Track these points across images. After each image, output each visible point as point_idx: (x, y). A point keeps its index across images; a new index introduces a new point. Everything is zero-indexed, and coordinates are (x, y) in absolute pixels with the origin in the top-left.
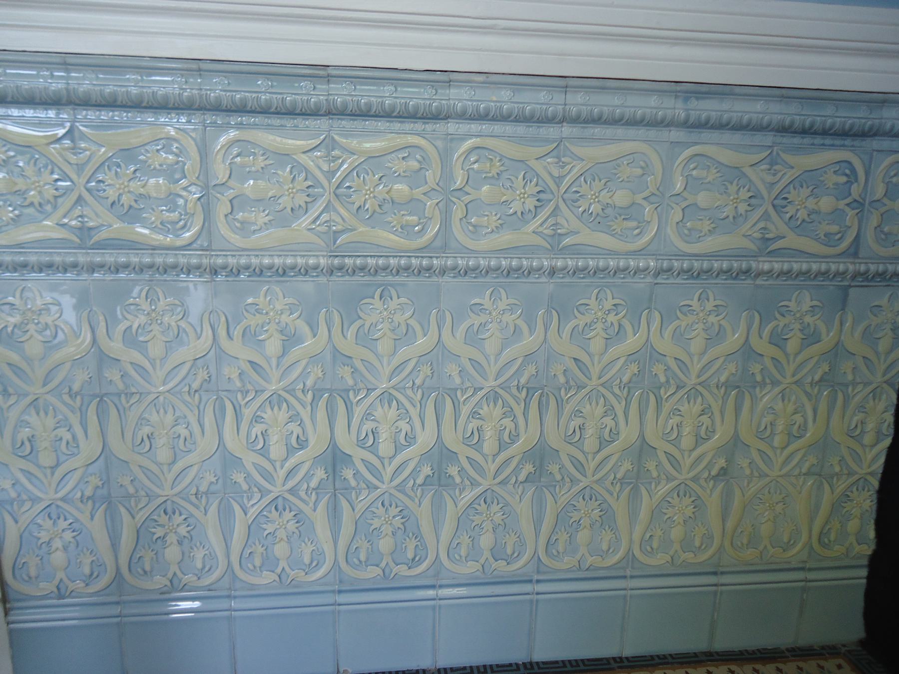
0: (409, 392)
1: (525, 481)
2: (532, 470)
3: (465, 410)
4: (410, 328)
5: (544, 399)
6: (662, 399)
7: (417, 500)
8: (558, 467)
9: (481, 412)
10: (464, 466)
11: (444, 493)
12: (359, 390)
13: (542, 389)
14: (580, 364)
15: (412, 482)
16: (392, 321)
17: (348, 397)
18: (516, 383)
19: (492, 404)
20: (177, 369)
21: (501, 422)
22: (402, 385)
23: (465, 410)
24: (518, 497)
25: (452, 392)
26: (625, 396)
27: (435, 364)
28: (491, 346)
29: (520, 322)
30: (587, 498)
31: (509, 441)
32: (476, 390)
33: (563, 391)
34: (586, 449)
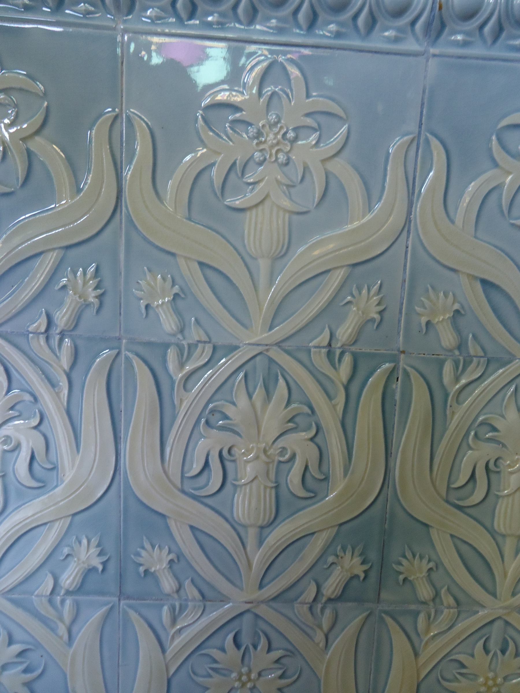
1: (339, 598)
2: (359, 571)
3: (188, 404)
4: (36, 167)
5: (397, 387)
7: (62, 630)
8: (425, 566)
9: (230, 410)
10: (186, 552)
11: (133, 615)
12: (192, 347)
13: (394, 359)
14: (498, 298)
15: (313, 589)
17: (164, 361)
18: (324, 338)
19: (259, 393)
21: (281, 443)
23: (188, 404)
24: (319, 637)
25: (153, 353)
26: (344, 378)
27: (106, 272)
28: (261, 230)
29: (340, 167)
30: (493, 646)
31: (302, 493)
32: (217, 351)
33: (448, 368)
34: (500, 524)
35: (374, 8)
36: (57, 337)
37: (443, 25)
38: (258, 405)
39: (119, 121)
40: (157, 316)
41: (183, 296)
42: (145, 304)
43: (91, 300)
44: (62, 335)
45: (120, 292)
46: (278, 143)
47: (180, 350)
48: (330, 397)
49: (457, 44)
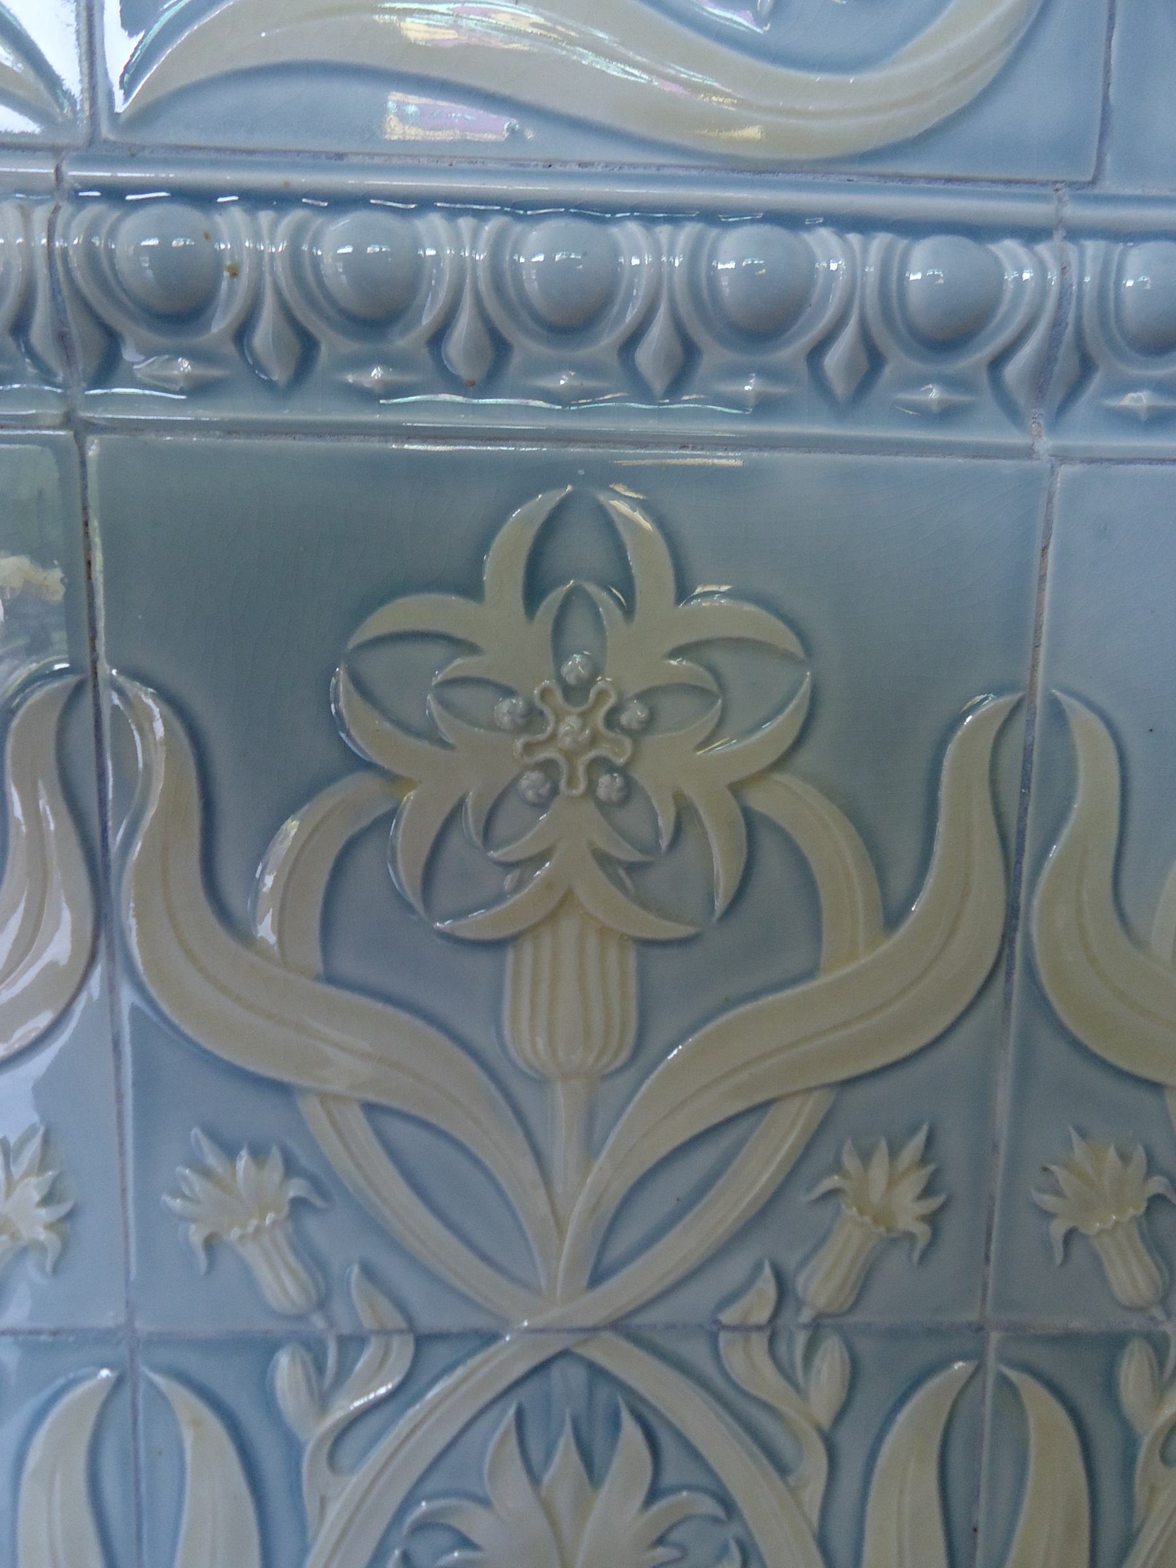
0: (750, 1364)
4: (772, 860)
6: (292, 1446)
9: (476, 1523)
12: (352, 1343)
16: (630, 789)
17: (1110, 1388)
20: (726, 1140)
22: (696, 1301)
29: (796, 805)
35: (492, 306)
36: (801, 1339)
37: (1087, 365)
38: (563, 1501)
39: (1023, 716)
40: (1096, 1261)
41: (319, 1203)
42: (206, 1232)
43: (42, 1235)
44: (816, 1329)
45: (992, 1198)
46: (594, 741)
47: (1155, 1348)
48: (783, 1470)
49: (1128, 420)
